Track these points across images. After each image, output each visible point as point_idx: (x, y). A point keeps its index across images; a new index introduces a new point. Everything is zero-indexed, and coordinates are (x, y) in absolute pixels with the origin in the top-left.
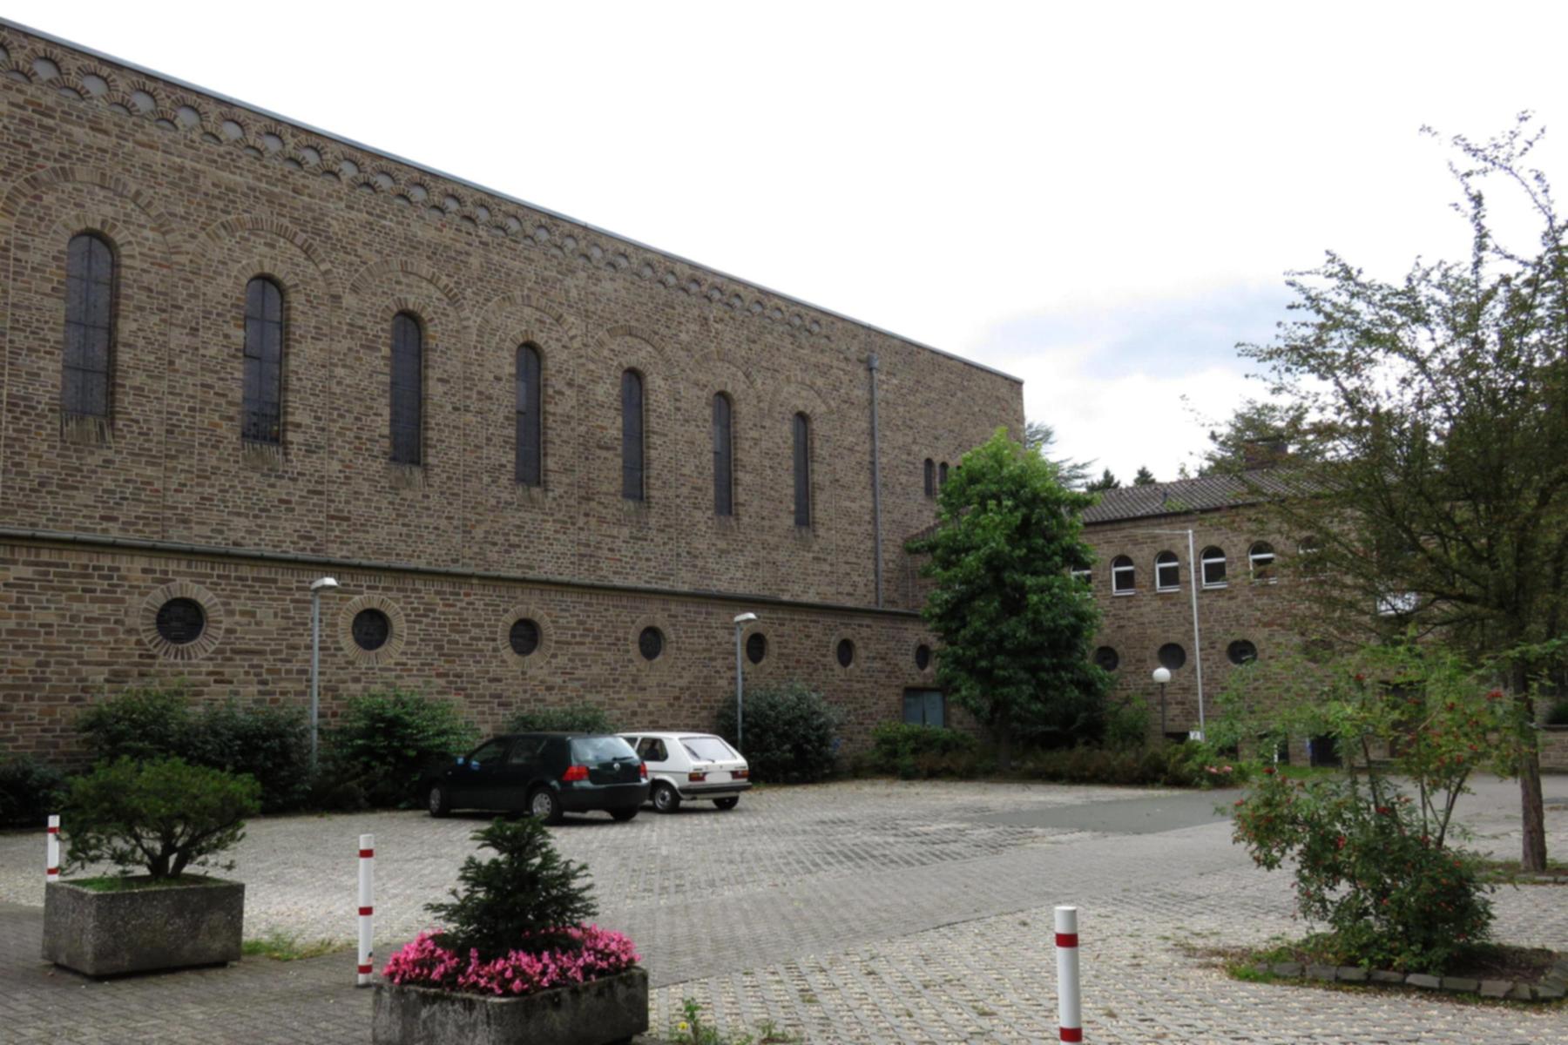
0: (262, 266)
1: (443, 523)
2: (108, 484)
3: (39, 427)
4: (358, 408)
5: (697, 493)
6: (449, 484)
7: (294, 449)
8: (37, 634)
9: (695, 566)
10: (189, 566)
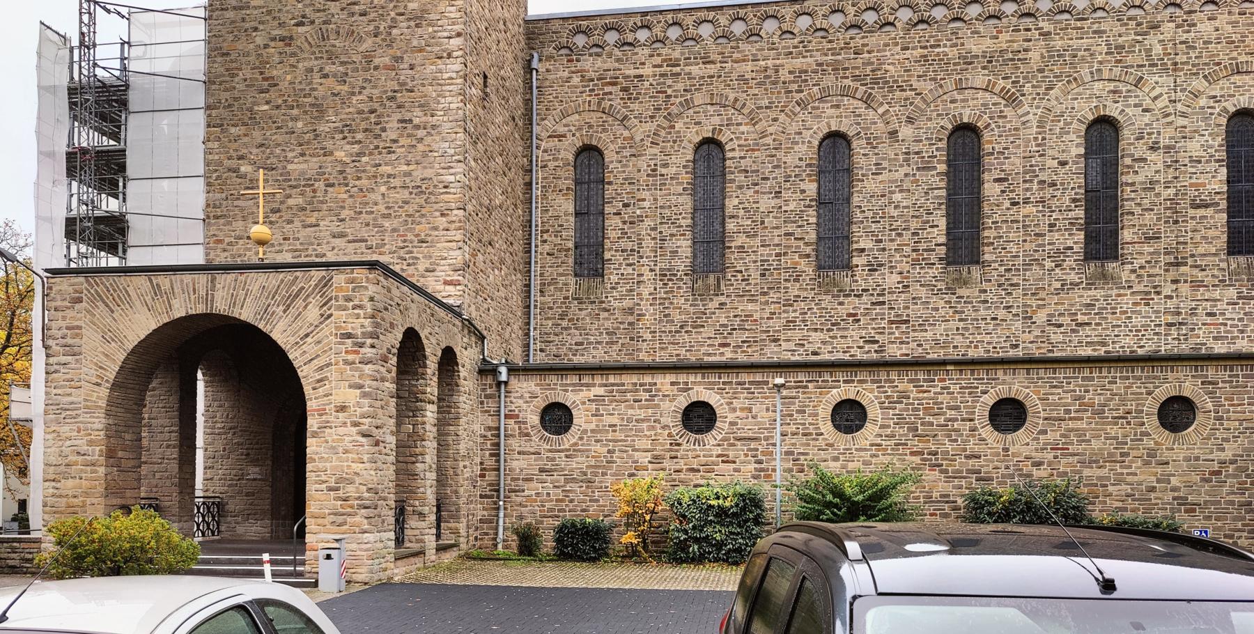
1: (1001, 314)
2: (723, 321)
3: (679, 288)
4: (914, 224)
8: (607, 431)
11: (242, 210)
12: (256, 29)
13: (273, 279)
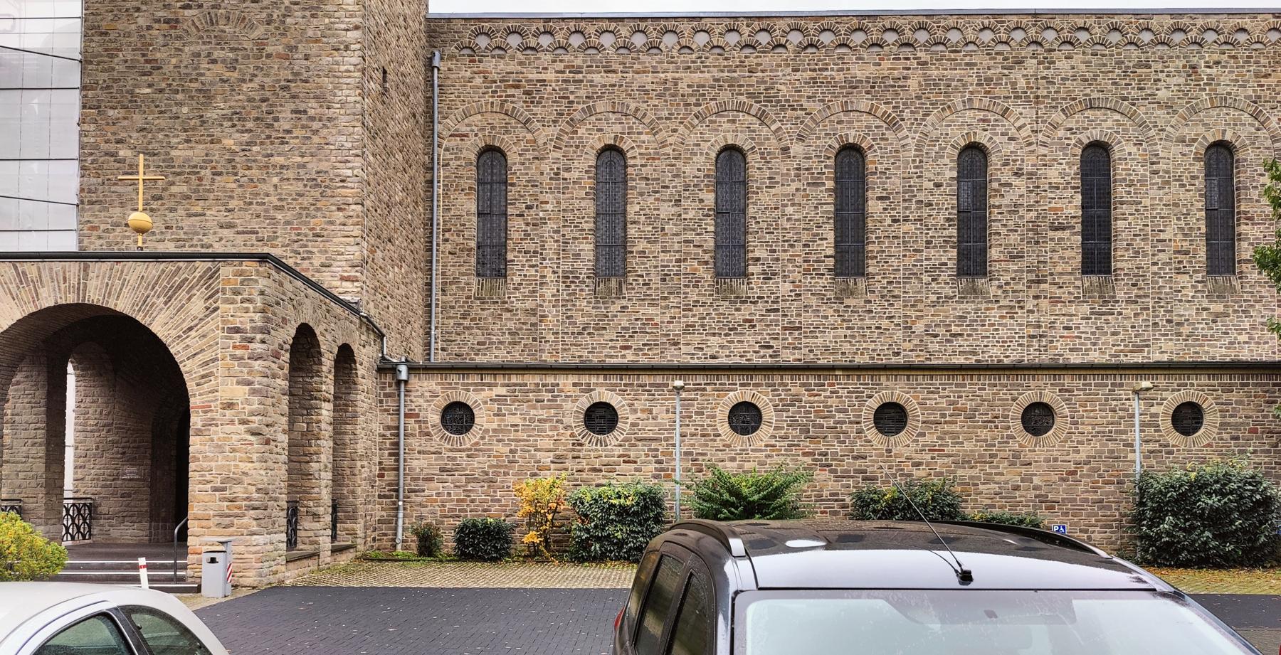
0: (726, 140)
1: (885, 323)
4: (805, 237)
5: (1181, 257)
6: (890, 288)
7: (754, 279)
9: (1179, 334)
10: (859, 379)
11: (120, 195)
12: (138, 10)
13: (154, 269)
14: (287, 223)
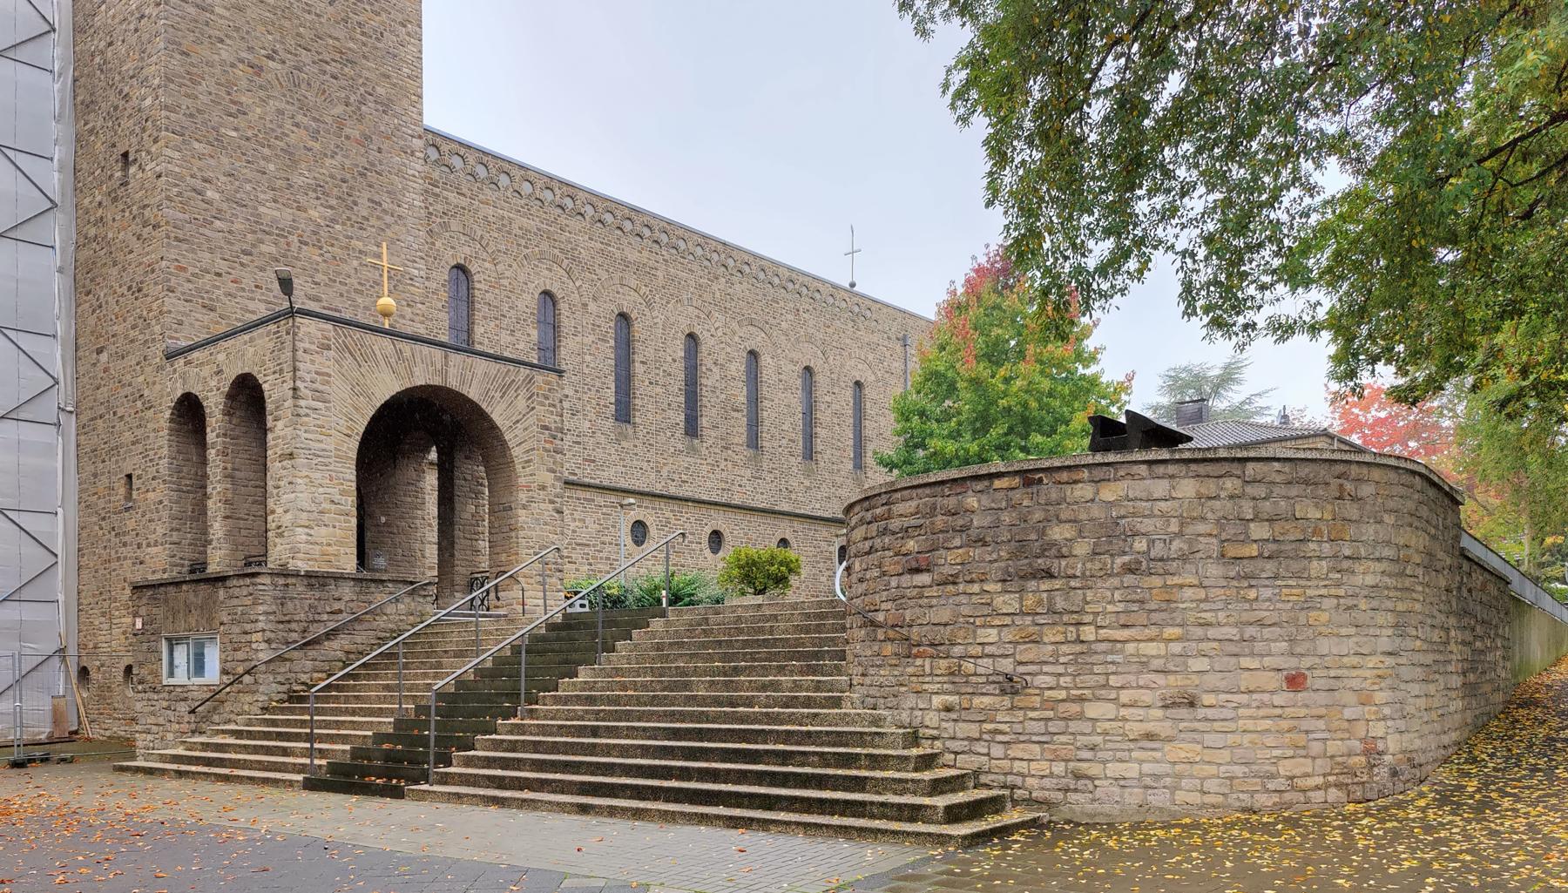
11: (209, 240)
12: (222, 41)
13: (494, 367)
14: (366, 308)
